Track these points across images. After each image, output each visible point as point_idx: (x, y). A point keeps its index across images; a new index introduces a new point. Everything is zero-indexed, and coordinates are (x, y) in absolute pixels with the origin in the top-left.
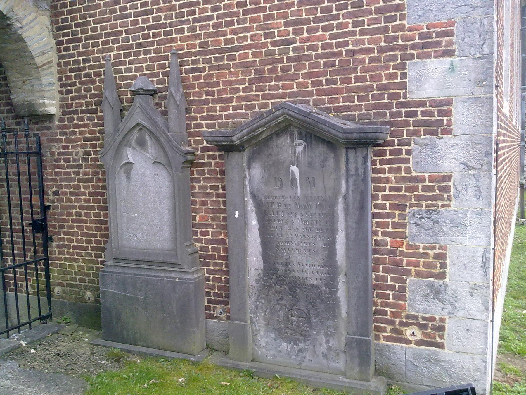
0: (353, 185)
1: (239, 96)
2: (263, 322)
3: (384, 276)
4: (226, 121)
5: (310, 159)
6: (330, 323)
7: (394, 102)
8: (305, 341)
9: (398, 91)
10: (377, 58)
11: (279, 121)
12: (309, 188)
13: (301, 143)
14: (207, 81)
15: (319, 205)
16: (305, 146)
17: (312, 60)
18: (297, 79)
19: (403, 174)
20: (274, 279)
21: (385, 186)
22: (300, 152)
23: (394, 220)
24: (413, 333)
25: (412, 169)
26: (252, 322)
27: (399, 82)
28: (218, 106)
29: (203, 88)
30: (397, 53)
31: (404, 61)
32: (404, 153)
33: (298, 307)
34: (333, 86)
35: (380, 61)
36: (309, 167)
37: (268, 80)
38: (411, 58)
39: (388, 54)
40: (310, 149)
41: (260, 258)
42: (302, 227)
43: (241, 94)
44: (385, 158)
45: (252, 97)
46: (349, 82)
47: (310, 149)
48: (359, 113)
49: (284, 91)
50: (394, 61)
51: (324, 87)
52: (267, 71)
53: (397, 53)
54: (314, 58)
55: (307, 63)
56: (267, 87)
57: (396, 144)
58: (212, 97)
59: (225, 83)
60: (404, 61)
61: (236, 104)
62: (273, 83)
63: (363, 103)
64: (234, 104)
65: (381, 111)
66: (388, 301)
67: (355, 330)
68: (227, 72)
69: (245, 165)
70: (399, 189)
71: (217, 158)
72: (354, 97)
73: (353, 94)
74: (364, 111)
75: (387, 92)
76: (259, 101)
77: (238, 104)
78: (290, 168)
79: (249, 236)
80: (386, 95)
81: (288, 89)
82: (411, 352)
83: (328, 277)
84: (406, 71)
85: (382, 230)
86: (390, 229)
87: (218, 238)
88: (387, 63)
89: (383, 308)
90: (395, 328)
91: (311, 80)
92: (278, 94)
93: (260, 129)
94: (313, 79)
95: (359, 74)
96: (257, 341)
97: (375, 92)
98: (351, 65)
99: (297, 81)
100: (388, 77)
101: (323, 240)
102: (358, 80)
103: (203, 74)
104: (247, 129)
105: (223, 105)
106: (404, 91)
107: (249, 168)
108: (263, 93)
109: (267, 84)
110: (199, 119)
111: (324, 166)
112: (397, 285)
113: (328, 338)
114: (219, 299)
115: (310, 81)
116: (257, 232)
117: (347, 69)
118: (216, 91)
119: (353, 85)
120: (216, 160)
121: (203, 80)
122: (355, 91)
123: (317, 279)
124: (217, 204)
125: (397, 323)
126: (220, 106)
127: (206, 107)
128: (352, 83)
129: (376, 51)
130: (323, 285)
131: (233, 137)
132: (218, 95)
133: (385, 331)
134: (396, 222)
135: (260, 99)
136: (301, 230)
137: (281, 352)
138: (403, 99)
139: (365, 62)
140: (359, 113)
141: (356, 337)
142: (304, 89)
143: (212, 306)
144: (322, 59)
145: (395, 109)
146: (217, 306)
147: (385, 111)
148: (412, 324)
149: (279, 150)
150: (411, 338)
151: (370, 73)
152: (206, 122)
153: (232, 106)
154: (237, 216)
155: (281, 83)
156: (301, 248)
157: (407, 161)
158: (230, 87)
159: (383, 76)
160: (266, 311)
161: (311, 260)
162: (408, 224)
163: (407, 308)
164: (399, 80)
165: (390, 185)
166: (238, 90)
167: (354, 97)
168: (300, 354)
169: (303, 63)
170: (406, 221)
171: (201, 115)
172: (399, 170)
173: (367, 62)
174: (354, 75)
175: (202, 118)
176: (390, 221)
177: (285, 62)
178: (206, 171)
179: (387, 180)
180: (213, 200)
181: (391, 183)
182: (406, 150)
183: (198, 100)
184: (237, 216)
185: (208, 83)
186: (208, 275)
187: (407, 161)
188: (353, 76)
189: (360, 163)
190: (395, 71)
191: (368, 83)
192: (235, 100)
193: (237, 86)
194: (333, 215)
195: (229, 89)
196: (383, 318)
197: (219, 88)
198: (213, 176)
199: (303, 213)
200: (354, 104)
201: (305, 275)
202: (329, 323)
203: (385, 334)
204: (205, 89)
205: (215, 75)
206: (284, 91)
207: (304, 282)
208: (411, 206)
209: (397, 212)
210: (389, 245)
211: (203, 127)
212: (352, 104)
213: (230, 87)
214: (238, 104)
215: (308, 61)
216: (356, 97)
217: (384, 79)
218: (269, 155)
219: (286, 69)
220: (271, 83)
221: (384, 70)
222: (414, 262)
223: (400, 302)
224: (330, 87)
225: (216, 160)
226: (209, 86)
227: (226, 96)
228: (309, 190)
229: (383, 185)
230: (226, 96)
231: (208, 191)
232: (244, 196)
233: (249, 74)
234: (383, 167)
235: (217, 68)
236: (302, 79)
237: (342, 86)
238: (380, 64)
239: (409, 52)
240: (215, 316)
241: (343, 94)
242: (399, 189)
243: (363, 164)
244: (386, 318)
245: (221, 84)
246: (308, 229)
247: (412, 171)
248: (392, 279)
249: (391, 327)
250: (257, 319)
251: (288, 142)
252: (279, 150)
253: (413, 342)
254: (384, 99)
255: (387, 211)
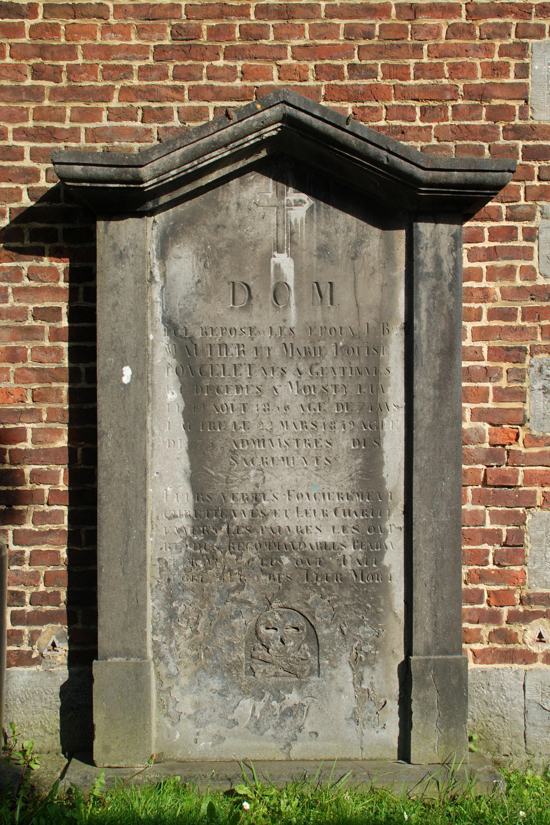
0: (429, 298)
1: (129, 87)
2: (189, 651)
3: (476, 511)
4: (88, 145)
5: (323, 237)
6: (366, 631)
7: (501, 125)
8: (300, 686)
9: (510, 103)
10: (467, 28)
11: (266, 135)
12: (319, 308)
13: (301, 200)
14: (40, 42)
15: (342, 348)
16: (311, 208)
17: (319, 17)
18: (280, 59)
19: (519, 282)
20: (222, 538)
21: (480, 309)
22: (299, 222)
23: (497, 384)
24: (540, 636)
25: (538, 271)
26: (159, 656)
27: (512, 84)
28: (69, 107)
29: (27, 58)
30: (508, 20)
31: (524, 40)
32: (520, 237)
33: (285, 603)
34: (366, 82)
35: (472, 35)
36: (319, 257)
37: (208, 53)
38: (538, 33)
39: (490, 21)
40: (322, 214)
41: (185, 489)
42: (298, 403)
43: (135, 82)
44: (480, 245)
45: (163, 92)
46: (404, 76)
47: (322, 214)
48: (423, 144)
49: (248, 83)
50: (502, 37)
51: (346, 82)
52: (205, 33)
53: (508, 20)
54: (323, 14)
55: (307, 25)
56: (205, 71)
57: (504, 217)
58: (52, 84)
59: (88, 51)
60: (524, 40)
61: (120, 105)
62: (220, 63)
63: (434, 125)
64: (115, 103)
65: (474, 143)
66: (485, 568)
67: (430, 640)
68: (99, 24)
69: (152, 247)
70: (509, 315)
71: (60, 238)
72: (413, 108)
73: (411, 103)
74: (434, 142)
75: (487, 104)
76: (182, 101)
77: (126, 105)
78: (273, 259)
79: (157, 431)
80: (484, 109)
81: (257, 80)
82: (537, 679)
83: (362, 520)
84: (527, 60)
85: (473, 406)
86: (491, 405)
87: (51, 446)
88: (486, 41)
89: (475, 586)
90: (501, 630)
91: (315, 63)
92: (232, 88)
93: (214, 154)
94: (319, 62)
95: (425, 60)
96: (171, 704)
97: (460, 102)
98: (409, 39)
99: (280, 62)
100: (490, 71)
101: (352, 431)
102: (423, 73)
103: (28, 23)
104: (182, 150)
105: (82, 105)
106: (522, 102)
107: (163, 255)
108: (192, 83)
109: (206, 64)
110: (10, 136)
111: (356, 254)
112: (504, 529)
113: (361, 670)
114: (49, 608)
115: (311, 66)
116: (178, 421)
117: (399, 47)
118: (65, 69)
119: (412, 82)
120: (58, 244)
121: (28, 37)
122: (417, 96)
123: (334, 528)
124: (54, 355)
125: (505, 618)
126: (73, 109)
127: (33, 106)
128: (410, 79)
129: (464, 13)
130: (350, 543)
131: (141, 169)
132: (69, 79)
133: (479, 640)
134: (504, 387)
135: (186, 97)
136: (295, 412)
137: (237, 724)
138: (520, 119)
139: (438, 34)
140: (423, 144)
141: (432, 657)
142: (299, 84)
143: (26, 629)
144: (343, 19)
145: (501, 142)
146: (44, 628)
147: (482, 143)
148: (537, 615)
149: (246, 214)
150: (534, 649)
151: (451, 60)
152: (33, 144)
153: (108, 109)
154: (126, 380)
155: (239, 64)
156: (294, 454)
157: (527, 254)
158: (105, 63)
159: (479, 67)
160: (197, 623)
161: (320, 483)
162: (528, 390)
163: (527, 581)
164: (511, 79)
165: (490, 305)
166: (127, 72)
167: (413, 108)
168: (289, 720)
169: (298, 22)
170: (525, 385)
171: (17, 126)
172: (509, 272)
173: (444, 35)
174: (416, 61)
175: (21, 134)
176: (490, 385)
177: (253, 17)
178: (25, 272)
179: (485, 296)
180: (43, 347)
181: (494, 301)
182: (524, 229)
183: (12, 88)
184: (126, 380)
185: (43, 48)
186: (18, 548)
187: (527, 254)
188: (412, 62)
189: (446, 249)
190: (504, 59)
191: (445, 81)
192: (116, 95)
193: (125, 62)
194: (377, 371)
195: (101, 67)
196: (474, 609)
197: (73, 62)
198: (46, 284)
199: (302, 369)
200: (414, 124)
201: (304, 521)
202: (364, 633)
203: (477, 647)
204: (32, 62)
205: (63, 28)
206: (248, 83)
207: (302, 538)
208: (534, 351)
209: (506, 366)
210: (487, 440)
211: (22, 158)
212: (408, 124)
213: (105, 63)
214: (126, 105)
215: (308, 18)
216: (418, 110)
217: (479, 75)
218: (218, 226)
219: (254, 32)
220: (215, 63)
221: (481, 54)
222: (541, 475)
223: (512, 568)
224: (359, 82)
225: (58, 244)
226: (48, 55)
227: (93, 83)
228: (319, 313)
229: (476, 306)
230: (93, 83)
231: (30, 322)
232: (143, 329)
233: (157, 34)
234: (476, 265)
235: (71, 12)
236: (294, 58)
237: (388, 82)
238: (472, 42)
239: (534, 20)
240: (34, 656)
241: (389, 100)
242: (509, 315)
243: (452, 251)
244: (479, 609)
245: (80, 52)
246: (313, 406)
247: (538, 275)
248: (496, 517)
249: (493, 627)
250: (173, 645)
251: (270, 195)
252: (246, 214)
253: (540, 657)
254: (479, 118)
255: (484, 364)
